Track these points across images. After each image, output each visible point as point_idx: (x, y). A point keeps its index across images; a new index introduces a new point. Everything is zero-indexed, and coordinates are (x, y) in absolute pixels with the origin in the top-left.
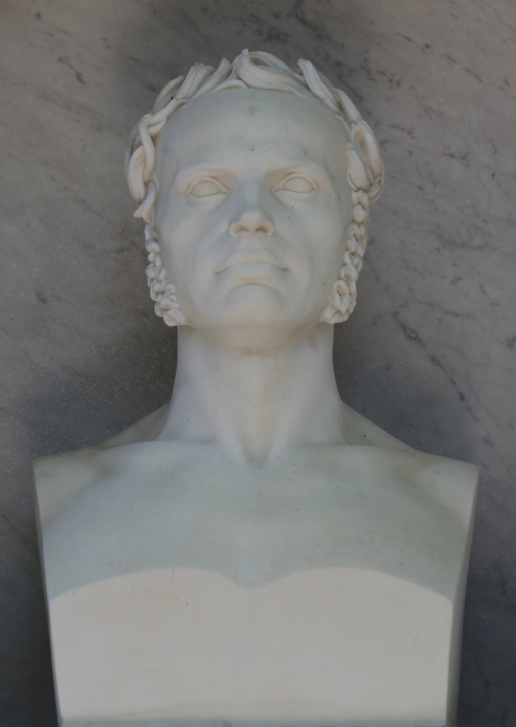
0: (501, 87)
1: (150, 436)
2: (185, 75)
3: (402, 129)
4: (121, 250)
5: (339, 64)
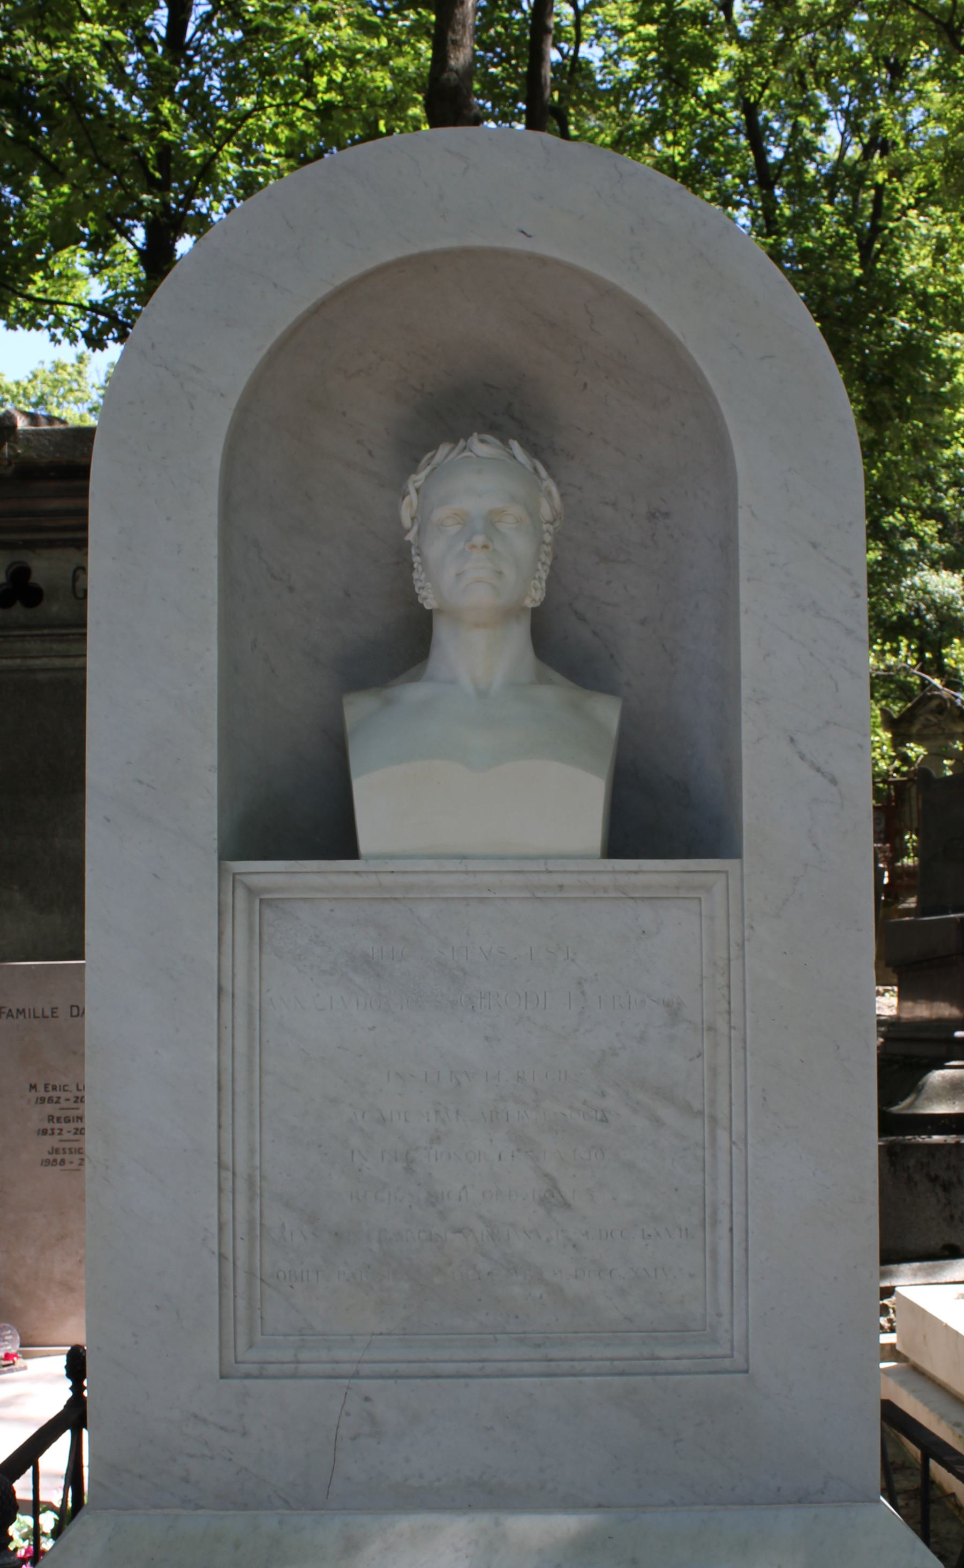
1: (416, 678)
2: (437, 449)
5: (535, 445)
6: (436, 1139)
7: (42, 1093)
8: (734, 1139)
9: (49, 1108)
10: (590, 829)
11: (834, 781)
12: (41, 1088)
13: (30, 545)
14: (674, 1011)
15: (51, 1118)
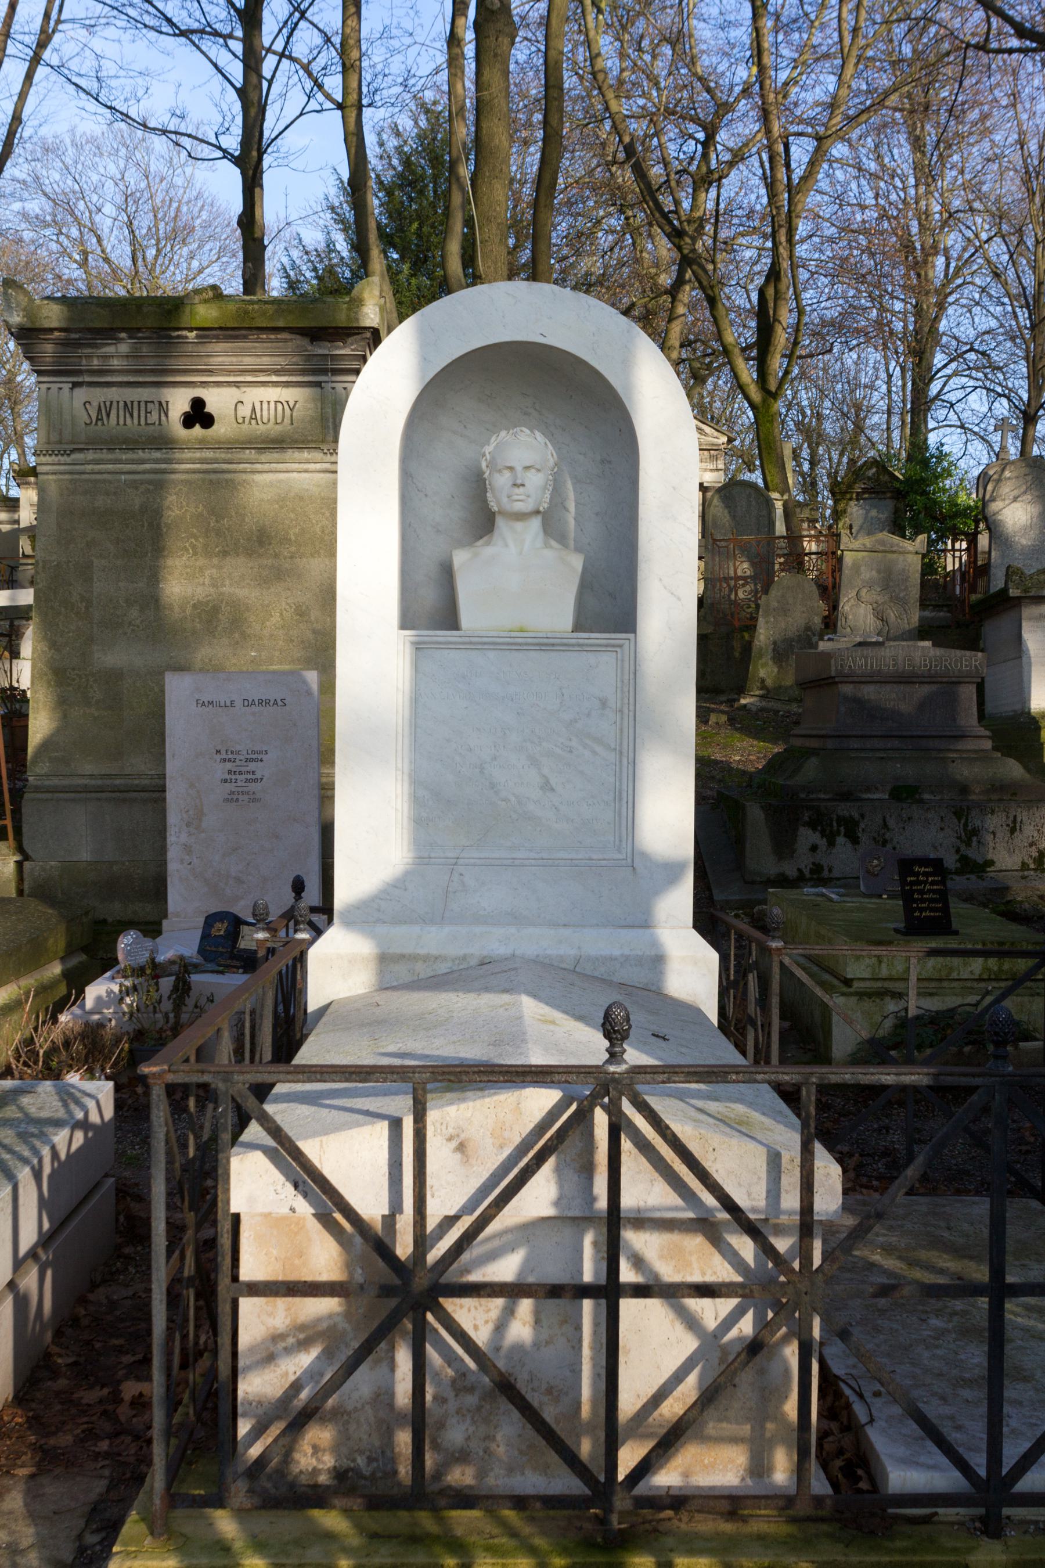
1: (488, 544)
6: (495, 758)
7: (224, 756)
9: (229, 766)
11: (679, 599)
12: (223, 752)
13: (204, 384)
14: (604, 703)
15: (230, 772)
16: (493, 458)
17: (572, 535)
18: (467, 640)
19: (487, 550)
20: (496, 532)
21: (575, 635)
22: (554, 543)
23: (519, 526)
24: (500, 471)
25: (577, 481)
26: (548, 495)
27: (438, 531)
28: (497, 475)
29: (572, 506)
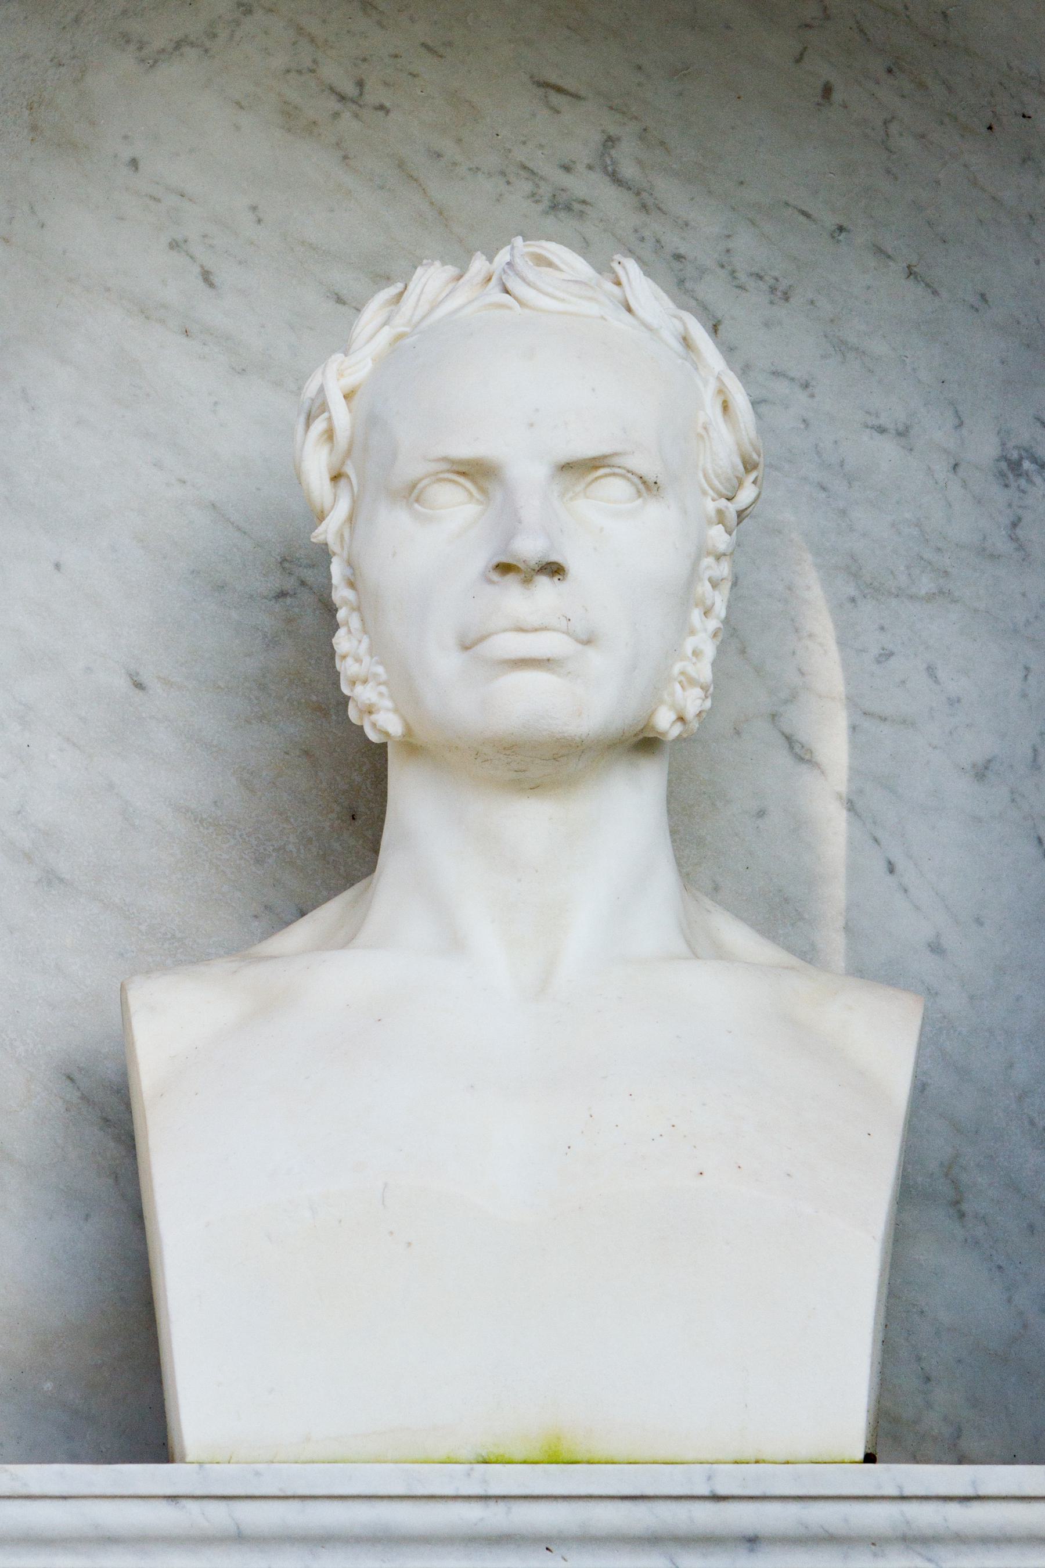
0: (972, 307)
1: (346, 938)
2: (406, 278)
3: (793, 379)
4: (282, 594)
5: (678, 257)
8: (208, 1466)
10: (846, 1414)
16: (372, 422)
17: (836, 894)
18: (218, 1515)
19: (338, 971)
20: (389, 859)
21: (889, 1476)
22: (736, 934)
23: (530, 821)
24: (412, 494)
25: (860, 584)
26: (703, 639)
27: (51, 878)
28: (393, 523)
29: (833, 742)
